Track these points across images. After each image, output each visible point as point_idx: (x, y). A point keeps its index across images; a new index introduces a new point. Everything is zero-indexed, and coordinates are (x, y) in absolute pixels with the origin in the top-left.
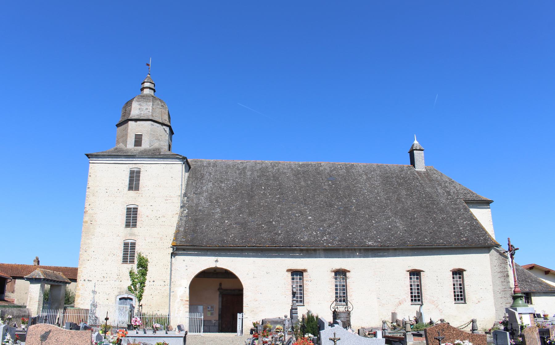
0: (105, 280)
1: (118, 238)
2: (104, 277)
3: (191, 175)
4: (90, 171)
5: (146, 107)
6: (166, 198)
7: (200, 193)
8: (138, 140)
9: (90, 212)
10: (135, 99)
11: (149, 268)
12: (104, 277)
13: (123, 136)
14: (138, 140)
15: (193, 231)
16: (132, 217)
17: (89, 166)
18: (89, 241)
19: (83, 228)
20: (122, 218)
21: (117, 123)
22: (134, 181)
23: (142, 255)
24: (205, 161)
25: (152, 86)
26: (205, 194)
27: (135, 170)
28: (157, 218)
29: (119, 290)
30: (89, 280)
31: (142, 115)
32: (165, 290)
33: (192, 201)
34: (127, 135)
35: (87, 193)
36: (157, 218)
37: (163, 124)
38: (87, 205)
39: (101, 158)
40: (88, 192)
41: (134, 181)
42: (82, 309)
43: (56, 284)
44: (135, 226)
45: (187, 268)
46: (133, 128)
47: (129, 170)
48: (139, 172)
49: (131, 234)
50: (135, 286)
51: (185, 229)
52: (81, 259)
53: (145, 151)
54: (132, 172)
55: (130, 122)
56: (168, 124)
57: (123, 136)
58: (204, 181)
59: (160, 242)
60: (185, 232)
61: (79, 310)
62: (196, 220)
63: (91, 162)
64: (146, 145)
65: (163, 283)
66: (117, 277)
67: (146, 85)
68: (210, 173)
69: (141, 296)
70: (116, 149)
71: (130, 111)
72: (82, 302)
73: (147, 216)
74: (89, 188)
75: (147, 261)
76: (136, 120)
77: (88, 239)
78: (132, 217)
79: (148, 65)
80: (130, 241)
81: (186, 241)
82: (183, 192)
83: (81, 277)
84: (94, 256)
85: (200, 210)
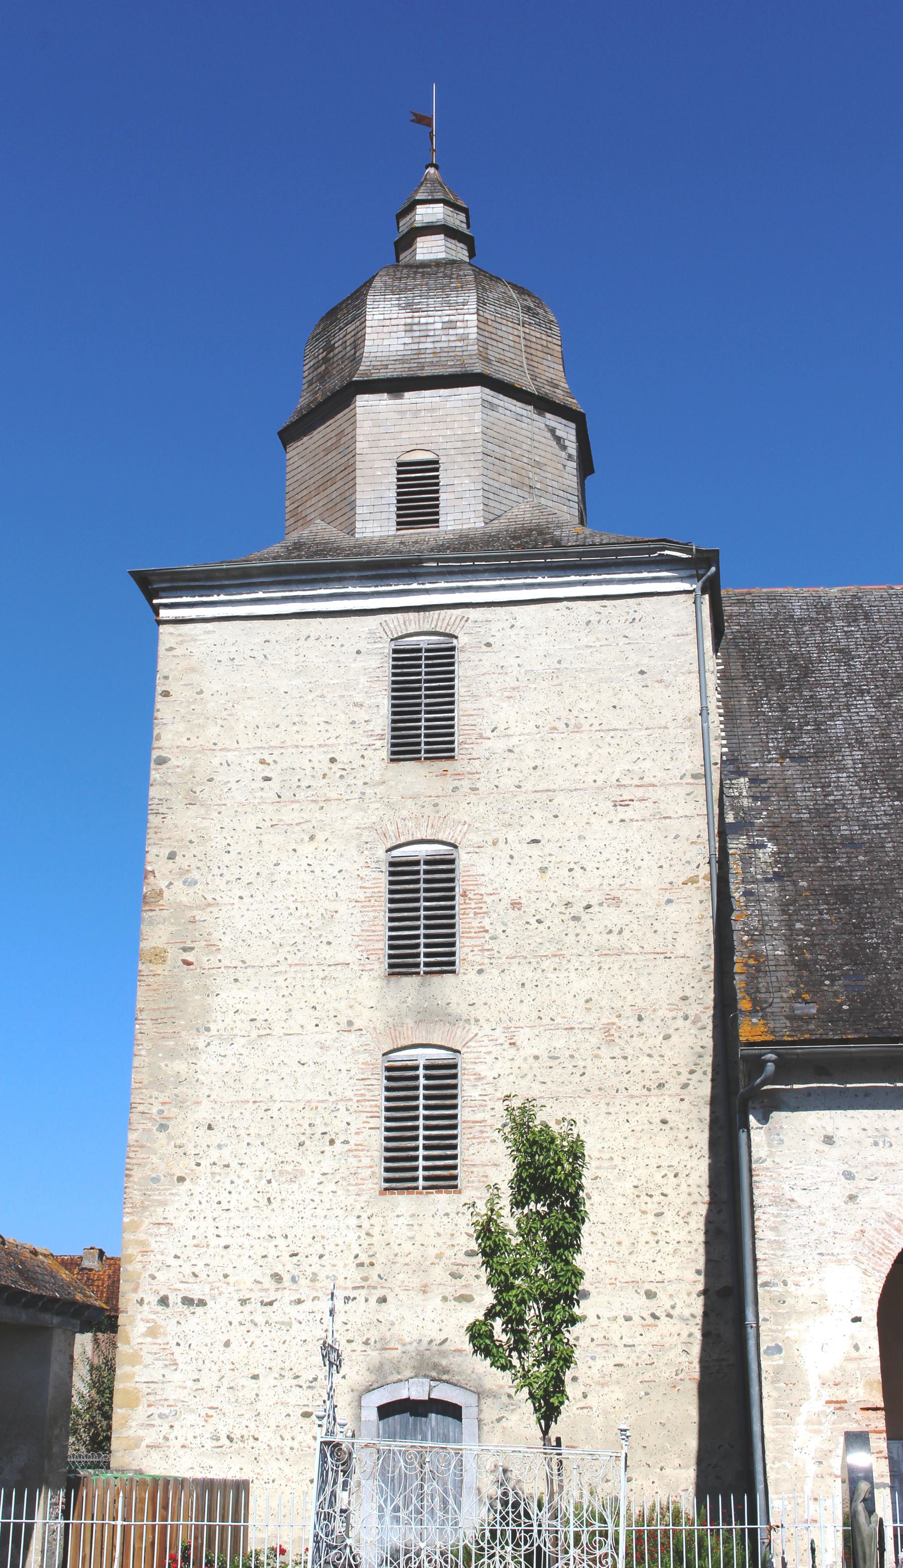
0: (288, 1296)
1: (352, 1037)
2: (277, 1278)
3: (736, 668)
4: (164, 665)
5: (448, 313)
6: (615, 794)
7: (819, 755)
8: (418, 488)
9: (178, 893)
10: (377, 283)
11: (596, 1203)
12: (277, 1278)
13: (327, 482)
14: (418, 488)
15: (851, 954)
16: (422, 912)
17: (155, 640)
18: (180, 1066)
19: (141, 992)
20: (362, 917)
21: (287, 418)
22: (422, 709)
23: (541, 1117)
24: (797, 597)
25: (457, 220)
26: (852, 757)
27: (423, 641)
28: (577, 909)
29: (374, 1355)
30: (188, 1301)
31: (429, 358)
32: (660, 1347)
33: (787, 793)
34: (349, 469)
35: (153, 792)
36: (577, 909)
37: (542, 404)
38: (155, 857)
39: (221, 589)
40: (161, 786)
41: (422, 709)
42: (181, 1483)
43: (23, 1317)
44: (444, 963)
45: (850, 1187)
46: (383, 431)
47: (387, 647)
48: (443, 658)
49: (426, 1015)
50: (515, 1324)
51: (793, 950)
52: (137, 1174)
53: (464, 542)
54: (404, 660)
55: (362, 400)
56: (573, 403)
57: (327, 482)
58: (823, 693)
59: (605, 1052)
60: (803, 965)
61: (161, 1492)
62: (843, 895)
63: (164, 614)
64: (461, 511)
65: (638, 1305)
66: (355, 1275)
67: (427, 214)
68: (846, 655)
69: (557, 1385)
70: (298, 546)
71: (358, 342)
72: (151, 1436)
73: (516, 905)
74: (162, 761)
75: (576, 1153)
76: (396, 386)
77: (172, 1054)
78: (422, 912)
79: (424, 121)
80: (422, 1056)
81: (830, 1015)
82: (717, 751)
83: (145, 1280)
84: (214, 1154)
85: (850, 842)
